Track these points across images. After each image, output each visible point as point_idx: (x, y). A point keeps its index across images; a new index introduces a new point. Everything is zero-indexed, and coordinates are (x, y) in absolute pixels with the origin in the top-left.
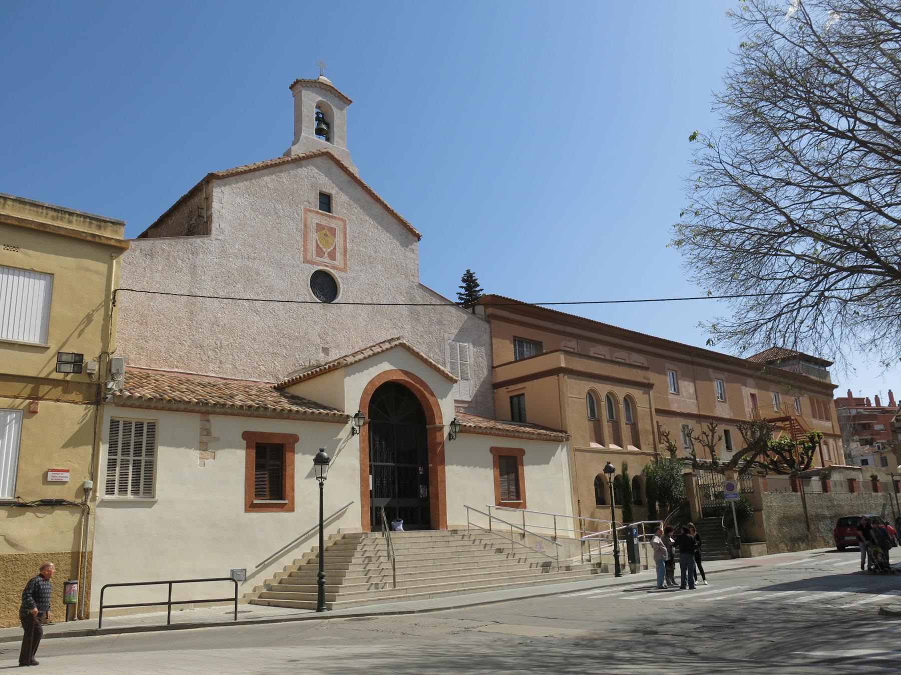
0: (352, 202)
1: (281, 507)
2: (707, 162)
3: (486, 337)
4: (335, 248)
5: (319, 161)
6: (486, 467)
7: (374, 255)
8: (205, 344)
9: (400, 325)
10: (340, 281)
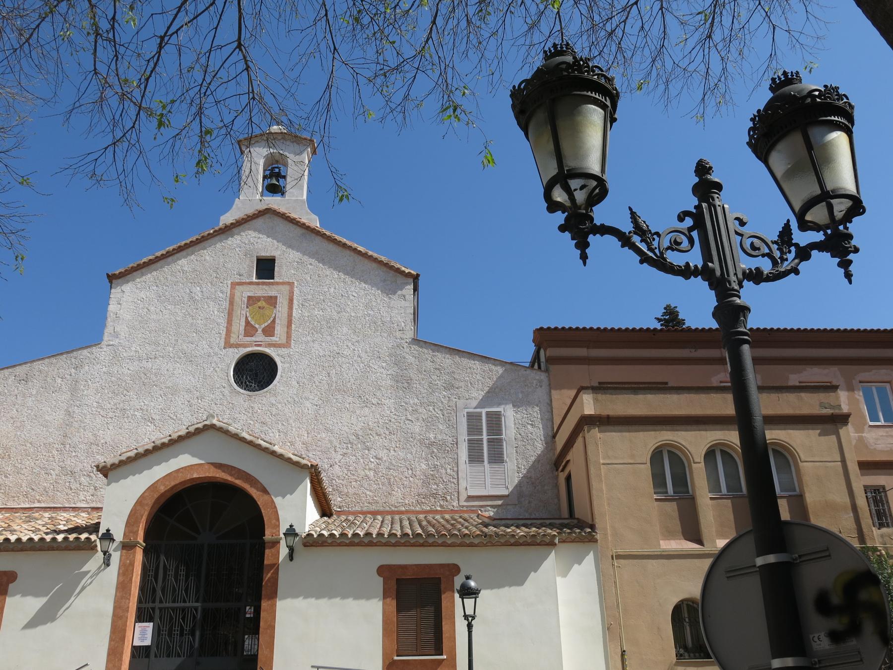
3: (541, 393)
4: (274, 321)
5: (259, 222)
6: (368, 598)
7: (335, 316)
8: (77, 469)
9: (375, 401)
10: (277, 360)
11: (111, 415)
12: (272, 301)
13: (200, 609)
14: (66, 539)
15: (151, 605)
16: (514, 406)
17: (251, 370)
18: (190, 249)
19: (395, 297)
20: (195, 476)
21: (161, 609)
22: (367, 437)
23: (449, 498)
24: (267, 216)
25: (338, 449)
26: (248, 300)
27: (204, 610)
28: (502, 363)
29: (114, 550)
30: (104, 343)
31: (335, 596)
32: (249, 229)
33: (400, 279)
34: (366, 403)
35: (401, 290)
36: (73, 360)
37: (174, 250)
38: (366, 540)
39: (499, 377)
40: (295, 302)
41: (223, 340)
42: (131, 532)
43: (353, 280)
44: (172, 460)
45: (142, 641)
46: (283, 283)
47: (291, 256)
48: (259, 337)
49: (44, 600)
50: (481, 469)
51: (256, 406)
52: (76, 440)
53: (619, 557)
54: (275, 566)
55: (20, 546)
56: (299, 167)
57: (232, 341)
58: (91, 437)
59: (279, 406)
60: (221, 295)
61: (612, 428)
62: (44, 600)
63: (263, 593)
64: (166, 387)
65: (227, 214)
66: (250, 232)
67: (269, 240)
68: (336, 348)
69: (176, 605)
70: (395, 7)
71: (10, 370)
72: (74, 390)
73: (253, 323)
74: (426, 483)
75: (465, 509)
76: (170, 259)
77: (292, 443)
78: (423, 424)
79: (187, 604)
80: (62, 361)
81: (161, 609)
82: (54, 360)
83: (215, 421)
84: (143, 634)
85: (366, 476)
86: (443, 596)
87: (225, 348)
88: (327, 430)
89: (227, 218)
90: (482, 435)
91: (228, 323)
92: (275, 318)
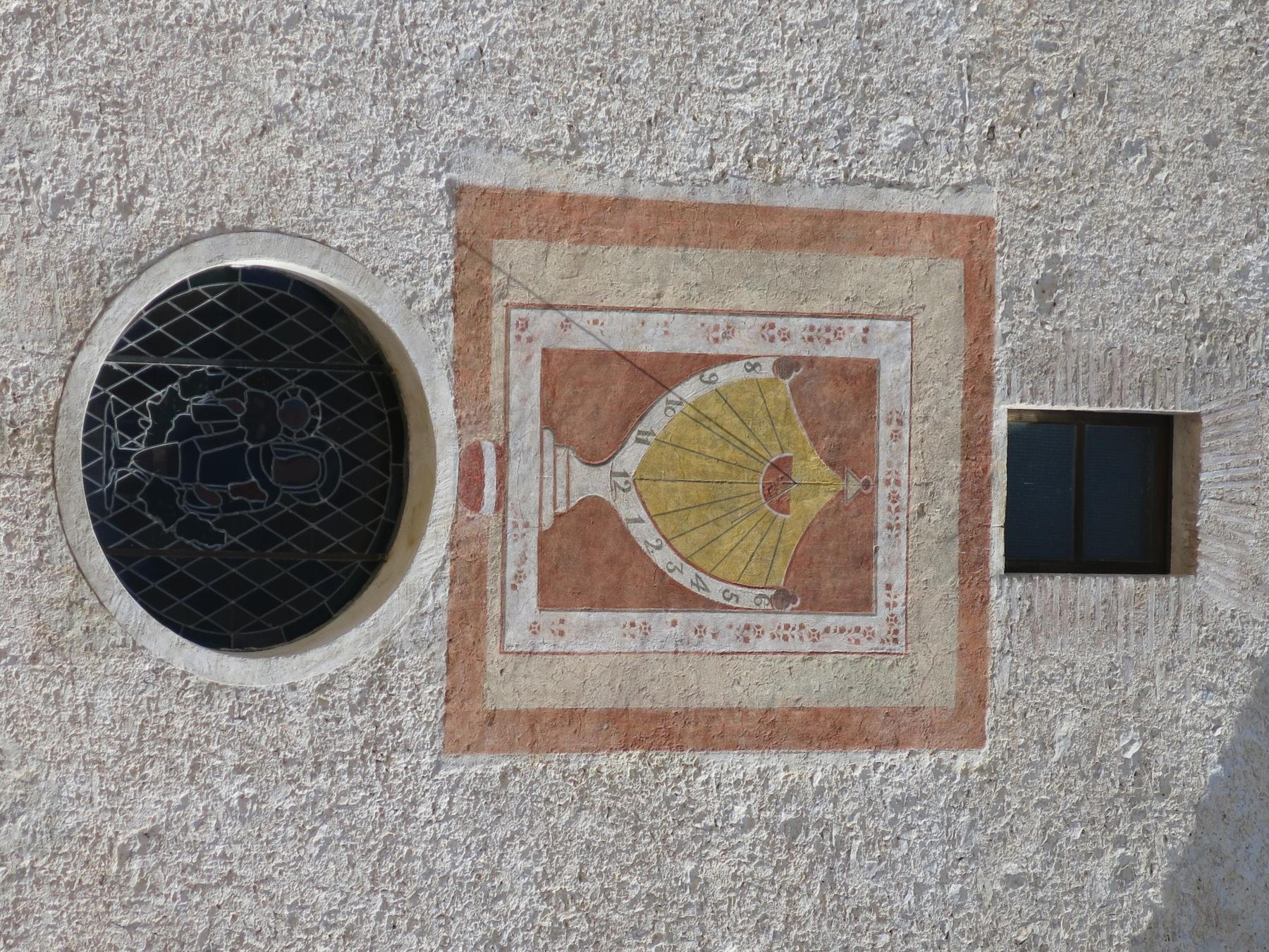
0: (1174, 827)
2: (730, 421)
4: (668, 595)
10: (342, 651)
12: (831, 571)
41: (521, 175)
46: (973, 654)
47: (1193, 708)
48: (542, 482)
57: (514, 255)
60: (890, 136)
70: (195, 888)
73: (657, 418)
87: (456, 193)
92: (690, 600)
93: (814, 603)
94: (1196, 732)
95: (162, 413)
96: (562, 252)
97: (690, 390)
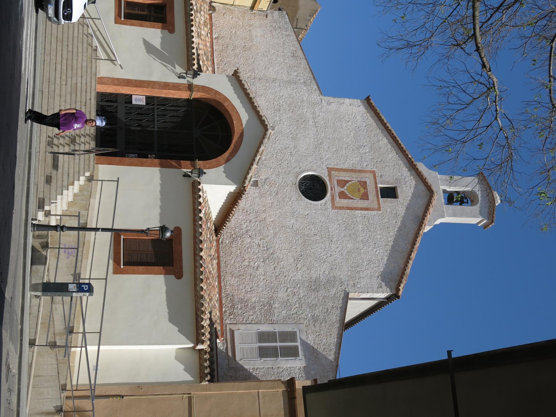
1: (118, 15)
4: (350, 198)
5: (422, 187)
9: (299, 266)
10: (323, 201)
11: (276, 103)
12: (365, 197)
13: (153, 129)
14: (194, 54)
15: (156, 103)
16: (304, 367)
17: (314, 186)
18: (395, 145)
19: (379, 280)
20: (235, 122)
21: (153, 109)
22: (272, 260)
23: (232, 317)
24: (428, 193)
25: (262, 241)
26: (363, 182)
27: (153, 131)
28: (337, 359)
29: (188, 81)
30: (323, 97)
31: (161, 202)
32: (416, 181)
33: (394, 285)
34: (297, 260)
35: (386, 285)
36: (309, 81)
37: (393, 134)
38: (197, 218)
39: (326, 358)
40: (366, 212)
41: (333, 167)
42: (199, 89)
43: (388, 252)
44: (244, 110)
45: (135, 99)
46: (379, 204)
48: (338, 189)
49: (159, 47)
50: (254, 341)
51: (289, 188)
52: (258, 85)
53: (190, 399)
54: (180, 167)
55: (189, 33)
56: (470, 217)
57: (333, 173)
58: (260, 94)
59: (290, 203)
60: (365, 165)
61: (287, 401)
62: (159, 47)
63: (163, 160)
64: (296, 134)
65: (424, 167)
66: (414, 182)
67: (411, 195)
68: (335, 239)
69: (156, 116)
71: (299, 48)
72: (290, 82)
73: (347, 185)
74: (241, 301)
75: (224, 328)
76: (386, 133)
77: (264, 211)
78: (285, 300)
79: (156, 123)
80: (309, 75)
81: (153, 109)
82: (308, 70)
83: (270, 131)
84: (139, 100)
85: (245, 260)
86: (161, 268)
88: (276, 234)
89: (421, 167)
90: (280, 342)
91: (345, 169)
93: (364, 199)
94: (402, 211)
95: (305, 185)
96: (337, 172)
97: (350, 183)
